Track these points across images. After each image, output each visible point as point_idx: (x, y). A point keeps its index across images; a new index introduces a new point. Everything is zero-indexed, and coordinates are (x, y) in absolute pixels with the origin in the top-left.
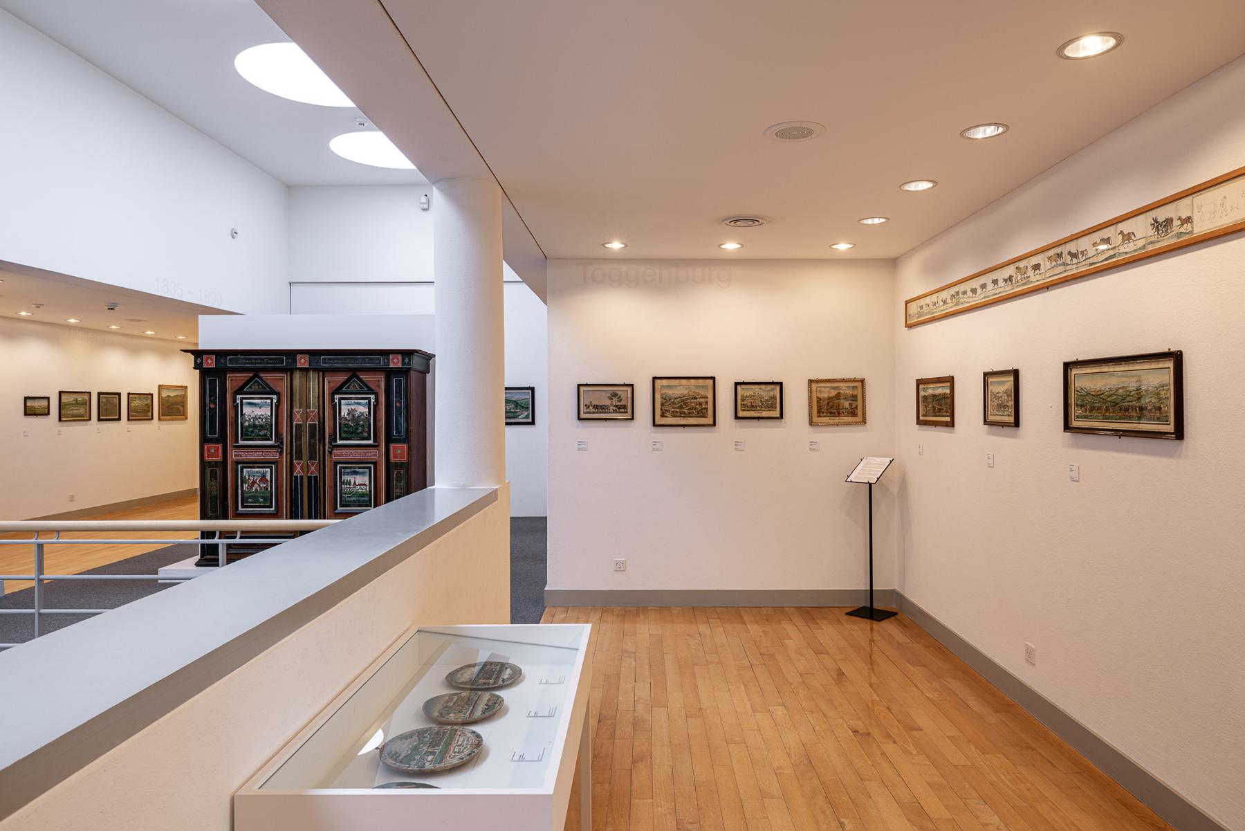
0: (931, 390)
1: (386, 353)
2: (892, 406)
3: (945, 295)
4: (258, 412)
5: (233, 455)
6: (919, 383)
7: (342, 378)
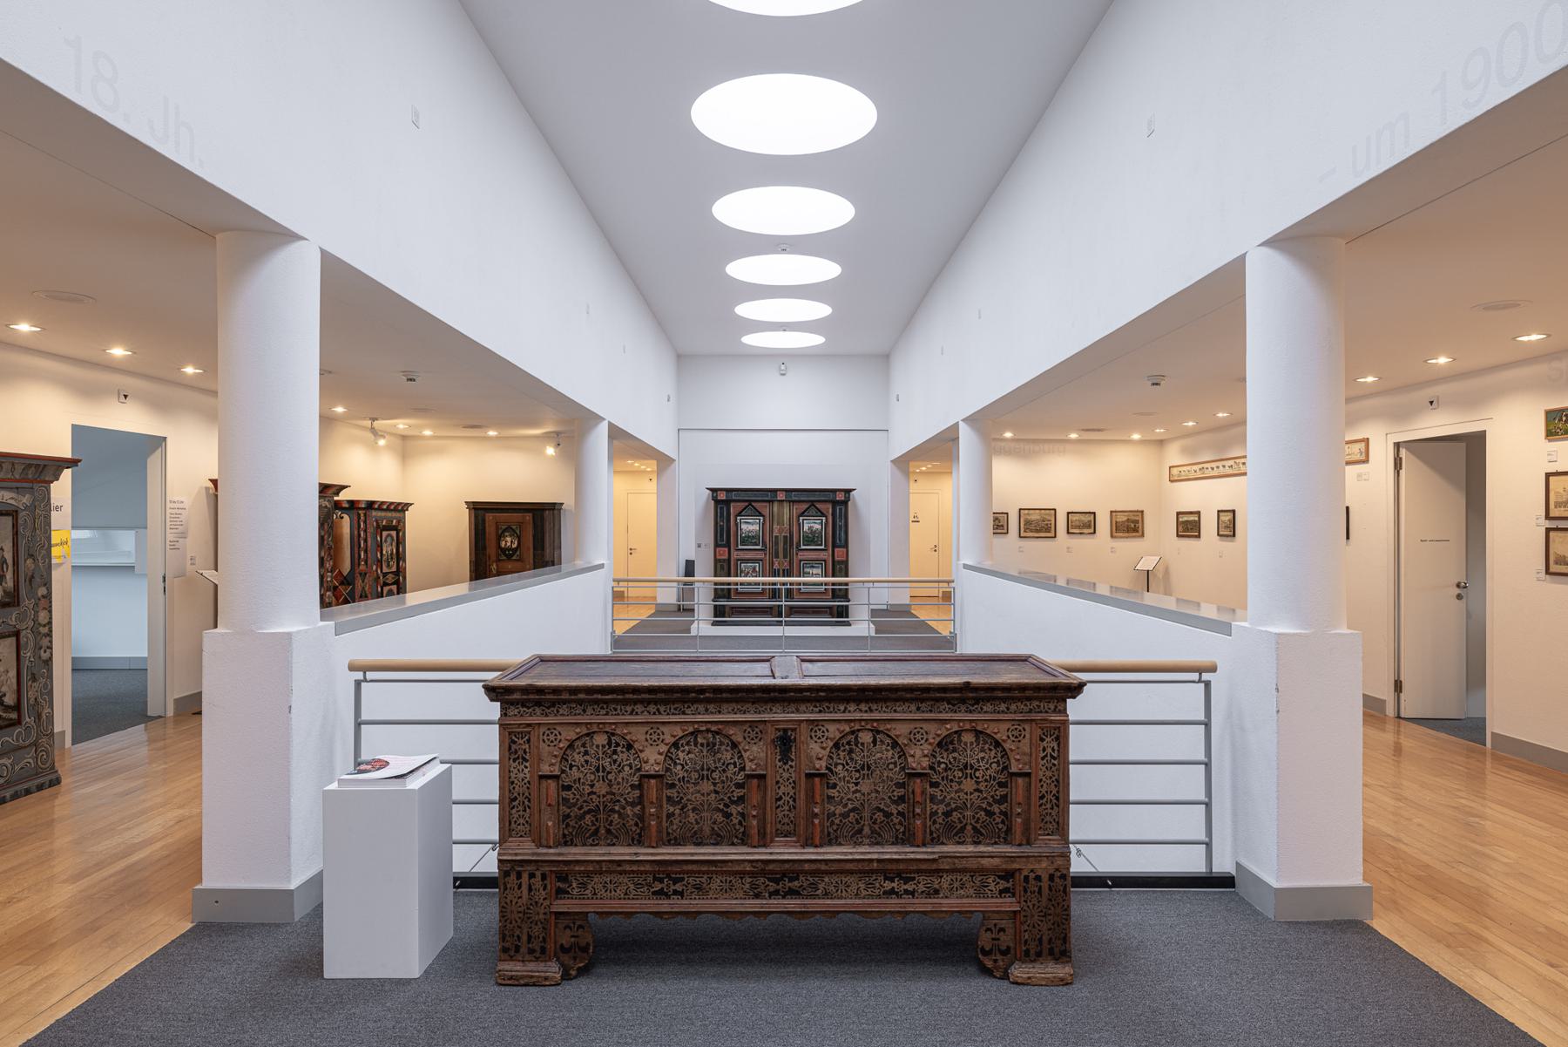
0: (1185, 518)
1: (834, 491)
2: (1160, 527)
3: (1196, 468)
4: (751, 527)
5: (735, 555)
6: (1178, 514)
7: (805, 506)
